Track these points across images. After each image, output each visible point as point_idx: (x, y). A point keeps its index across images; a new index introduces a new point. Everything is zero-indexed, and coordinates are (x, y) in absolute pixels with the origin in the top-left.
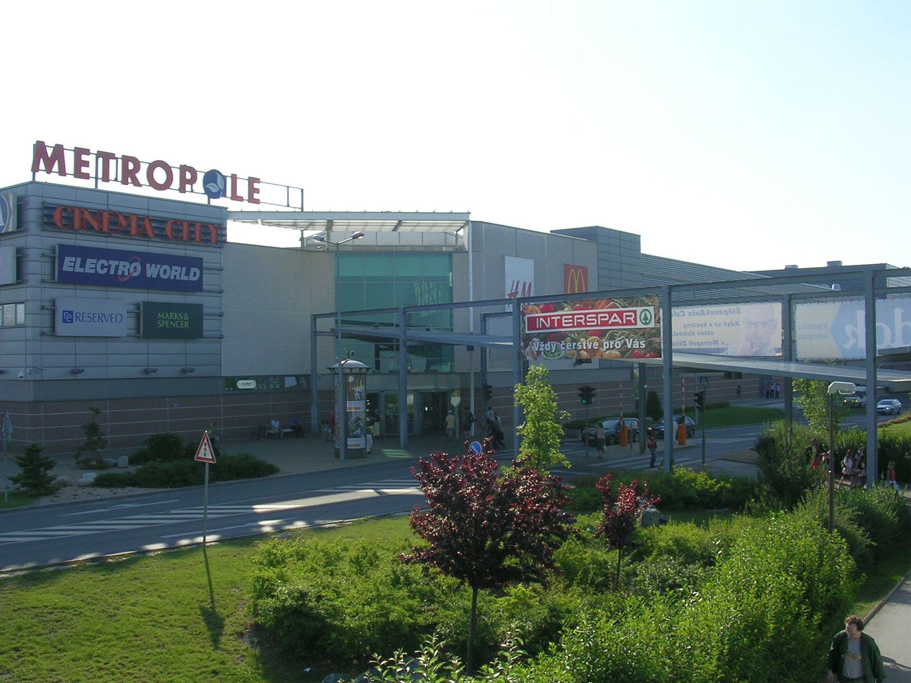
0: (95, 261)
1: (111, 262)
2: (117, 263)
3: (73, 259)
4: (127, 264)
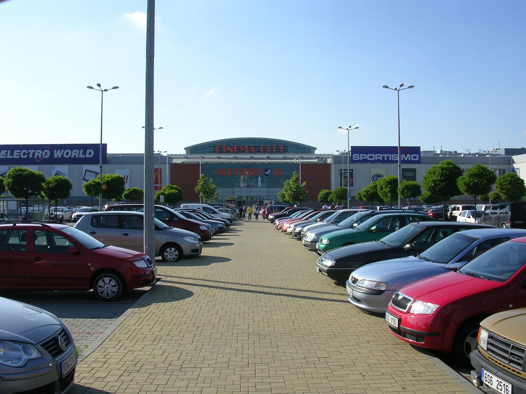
0: (19, 151)
1: (29, 151)
2: (34, 151)
3: (6, 151)
4: (40, 151)
